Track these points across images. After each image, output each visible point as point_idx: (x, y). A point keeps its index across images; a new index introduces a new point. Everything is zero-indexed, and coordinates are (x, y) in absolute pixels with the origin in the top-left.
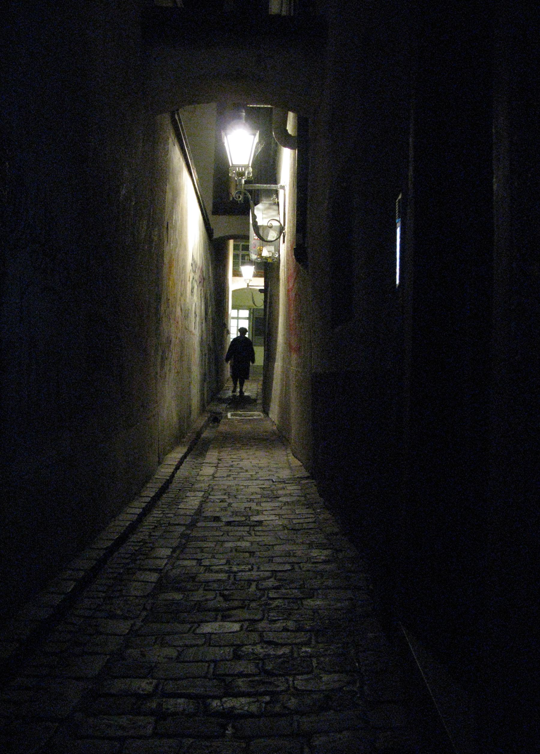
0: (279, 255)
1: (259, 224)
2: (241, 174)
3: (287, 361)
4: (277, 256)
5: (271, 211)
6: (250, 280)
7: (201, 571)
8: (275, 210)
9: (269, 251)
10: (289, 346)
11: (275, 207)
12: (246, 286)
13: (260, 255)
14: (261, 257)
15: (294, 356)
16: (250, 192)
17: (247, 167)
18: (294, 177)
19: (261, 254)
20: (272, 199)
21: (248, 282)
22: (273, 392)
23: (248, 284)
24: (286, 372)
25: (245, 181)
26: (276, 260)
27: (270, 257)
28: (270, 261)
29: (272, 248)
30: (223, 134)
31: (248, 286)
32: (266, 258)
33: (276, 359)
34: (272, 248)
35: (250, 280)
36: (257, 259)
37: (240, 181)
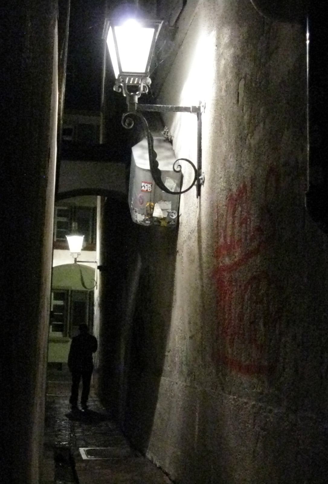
0: (178, 216)
2: (134, 88)
4: (175, 217)
6: (79, 254)
9: (162, 210)
11: (167, 145)
12: (72, 262)
13: (150, 214)
16: (147, 114)
17: (142, 76)
19: (152, 214)
20: (162, 133)
21: (76, 256)
23: (76, 259)
25: (139, 99)
26: (173, 223)
27: (164, 219)
29: (168, 206)
30: (107, 23)
31: (76, 261)
32: (159, 220)
34: (168, 206)
36: (144, 221)
37: (132, 98)
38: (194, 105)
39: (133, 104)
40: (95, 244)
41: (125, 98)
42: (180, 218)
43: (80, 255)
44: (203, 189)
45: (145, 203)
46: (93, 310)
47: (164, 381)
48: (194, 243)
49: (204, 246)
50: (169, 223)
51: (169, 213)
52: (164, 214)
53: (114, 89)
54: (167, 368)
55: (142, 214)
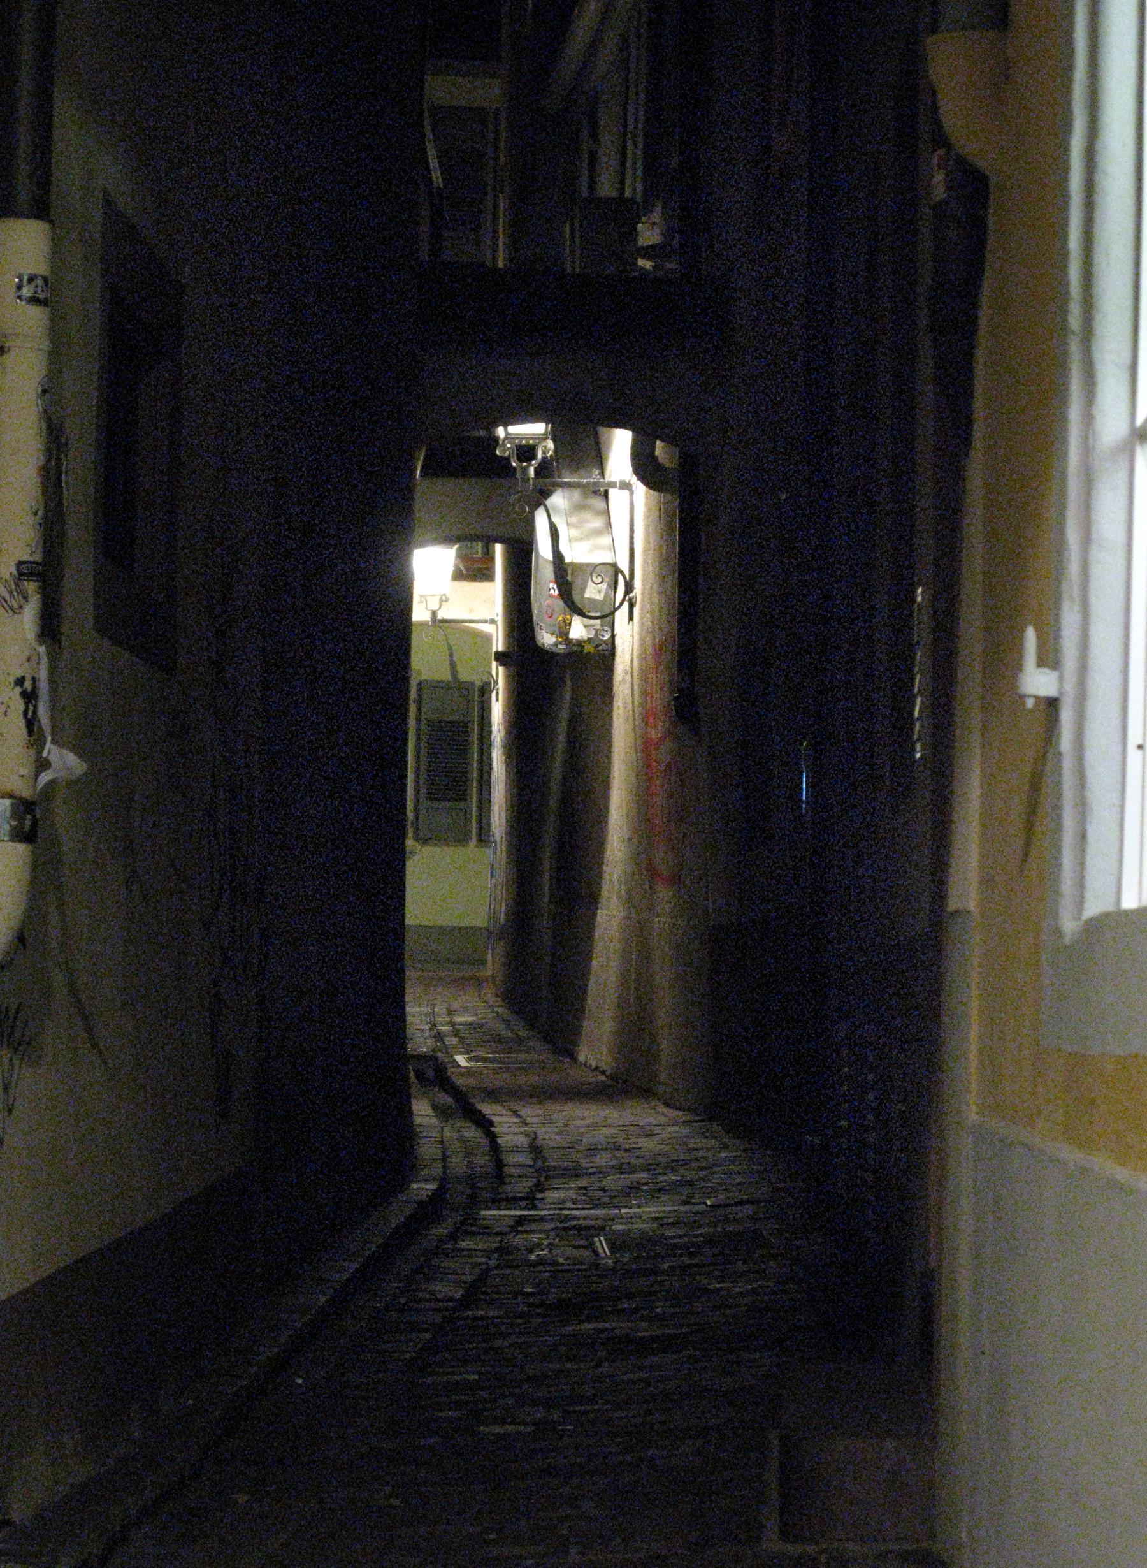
0: (613, 636)
1: (568, 560)
3: (639, 905)
4: (607, 637)
5: (588, 516)
7: (572, 1194)
8: (598, 513)
9: (585, 626)
10: (645, 870)
13: (564, 633)
14: (568, 641)
15: (664, 893)
18: (669, 525)
19: (568, 633)
22: (592, 988)
23: (434, 613)
24: (638, 934)
26: (604, 646)
28: (588, 648)
32: (580, 643)
33: (603, 901)
35: (443, 600)
36: (556, 644)
37: (525, 471)
38: (623, 478)
39: (526, 479)
40: (493, 559)
41: (515, 469)
42: (616, 639)
43: (447, 601)
44: (636, 610)
45: (555, 616)
46: (490, 758)
47: (601, 915)
48: (628, 692)
49: (636, 703)
50: (597, 646)
51: (597, 630)
52: (588, 633)
53: (498, 453)
54: (605, 893)
55: (552, 634)
